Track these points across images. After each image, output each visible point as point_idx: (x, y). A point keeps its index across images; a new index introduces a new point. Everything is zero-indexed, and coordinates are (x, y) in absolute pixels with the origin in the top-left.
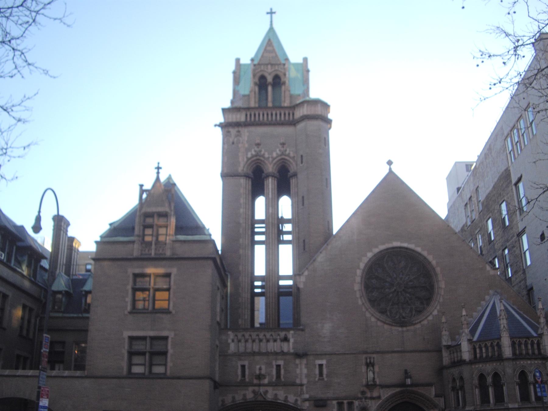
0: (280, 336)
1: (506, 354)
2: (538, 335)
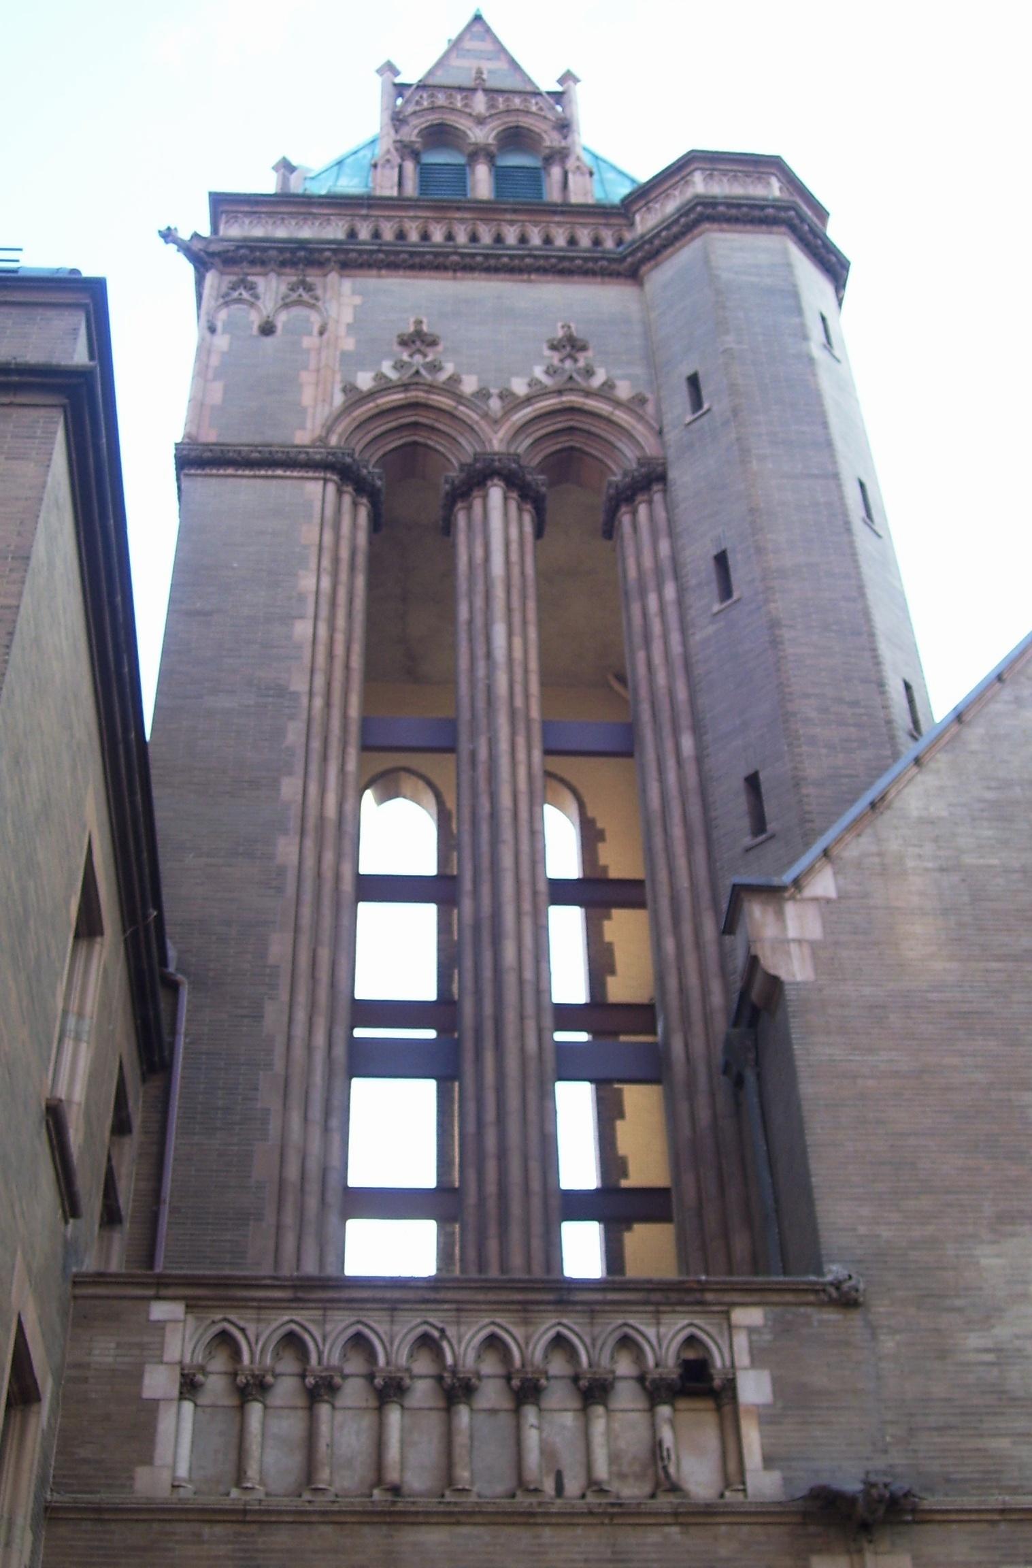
0: (639, 1356)
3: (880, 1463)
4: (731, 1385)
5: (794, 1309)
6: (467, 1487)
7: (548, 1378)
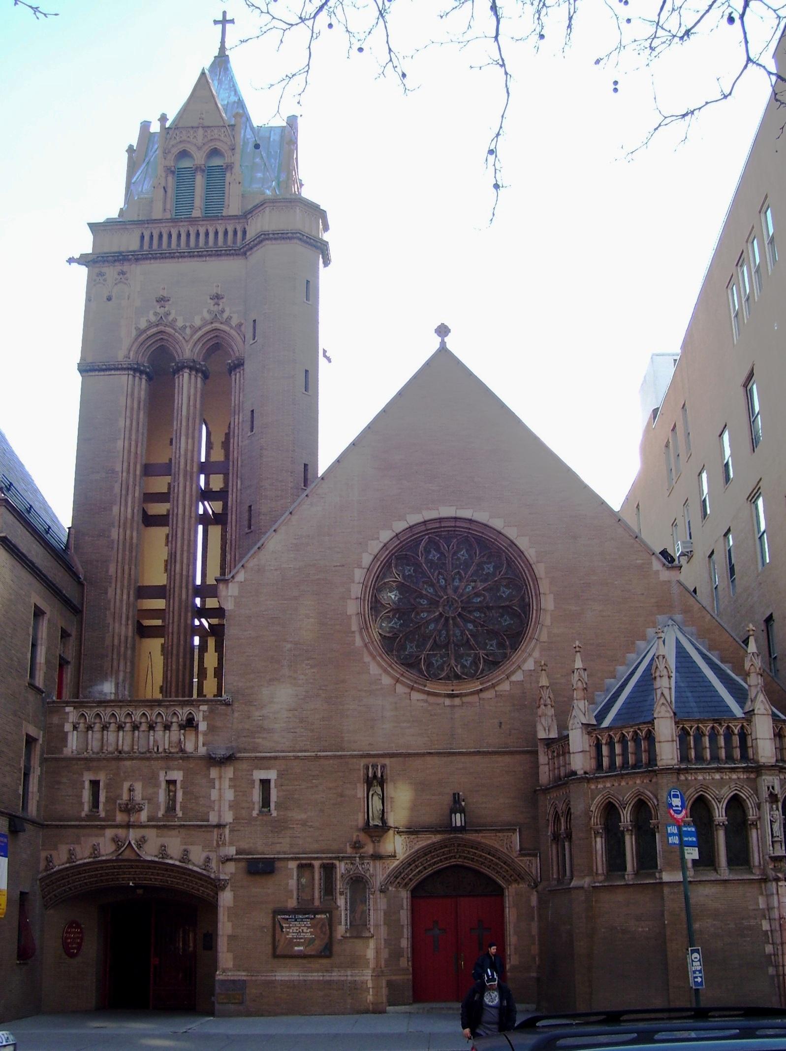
1: (663, 757)
2: (745, 713)
4: (198, 725)
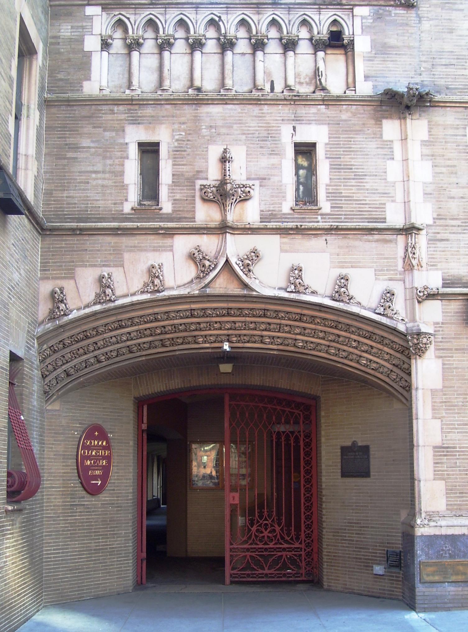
0: (310, 30)
3: (418, 80)
4: (352, 42)
5: (383, 8)
6: (230, 88)
7: (268, 39)
